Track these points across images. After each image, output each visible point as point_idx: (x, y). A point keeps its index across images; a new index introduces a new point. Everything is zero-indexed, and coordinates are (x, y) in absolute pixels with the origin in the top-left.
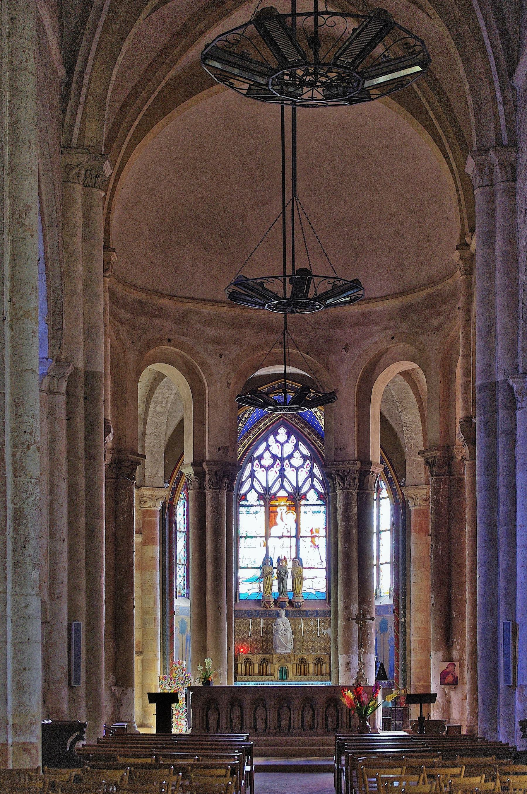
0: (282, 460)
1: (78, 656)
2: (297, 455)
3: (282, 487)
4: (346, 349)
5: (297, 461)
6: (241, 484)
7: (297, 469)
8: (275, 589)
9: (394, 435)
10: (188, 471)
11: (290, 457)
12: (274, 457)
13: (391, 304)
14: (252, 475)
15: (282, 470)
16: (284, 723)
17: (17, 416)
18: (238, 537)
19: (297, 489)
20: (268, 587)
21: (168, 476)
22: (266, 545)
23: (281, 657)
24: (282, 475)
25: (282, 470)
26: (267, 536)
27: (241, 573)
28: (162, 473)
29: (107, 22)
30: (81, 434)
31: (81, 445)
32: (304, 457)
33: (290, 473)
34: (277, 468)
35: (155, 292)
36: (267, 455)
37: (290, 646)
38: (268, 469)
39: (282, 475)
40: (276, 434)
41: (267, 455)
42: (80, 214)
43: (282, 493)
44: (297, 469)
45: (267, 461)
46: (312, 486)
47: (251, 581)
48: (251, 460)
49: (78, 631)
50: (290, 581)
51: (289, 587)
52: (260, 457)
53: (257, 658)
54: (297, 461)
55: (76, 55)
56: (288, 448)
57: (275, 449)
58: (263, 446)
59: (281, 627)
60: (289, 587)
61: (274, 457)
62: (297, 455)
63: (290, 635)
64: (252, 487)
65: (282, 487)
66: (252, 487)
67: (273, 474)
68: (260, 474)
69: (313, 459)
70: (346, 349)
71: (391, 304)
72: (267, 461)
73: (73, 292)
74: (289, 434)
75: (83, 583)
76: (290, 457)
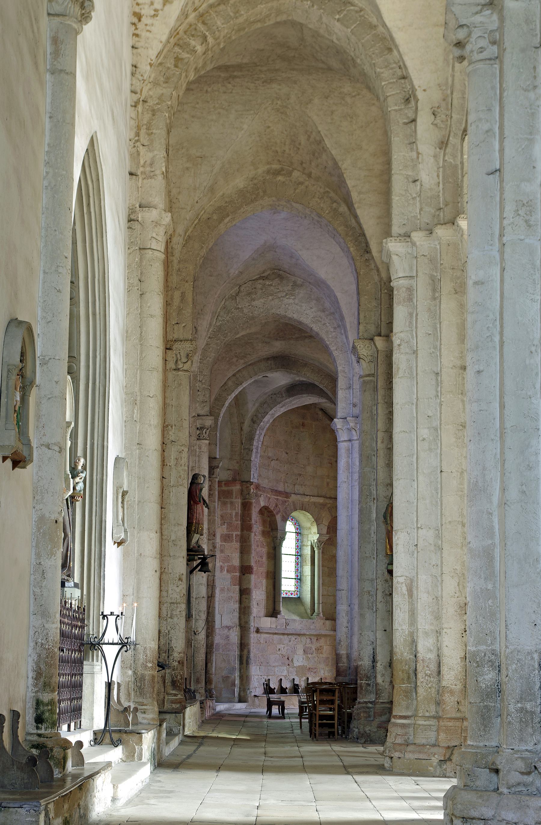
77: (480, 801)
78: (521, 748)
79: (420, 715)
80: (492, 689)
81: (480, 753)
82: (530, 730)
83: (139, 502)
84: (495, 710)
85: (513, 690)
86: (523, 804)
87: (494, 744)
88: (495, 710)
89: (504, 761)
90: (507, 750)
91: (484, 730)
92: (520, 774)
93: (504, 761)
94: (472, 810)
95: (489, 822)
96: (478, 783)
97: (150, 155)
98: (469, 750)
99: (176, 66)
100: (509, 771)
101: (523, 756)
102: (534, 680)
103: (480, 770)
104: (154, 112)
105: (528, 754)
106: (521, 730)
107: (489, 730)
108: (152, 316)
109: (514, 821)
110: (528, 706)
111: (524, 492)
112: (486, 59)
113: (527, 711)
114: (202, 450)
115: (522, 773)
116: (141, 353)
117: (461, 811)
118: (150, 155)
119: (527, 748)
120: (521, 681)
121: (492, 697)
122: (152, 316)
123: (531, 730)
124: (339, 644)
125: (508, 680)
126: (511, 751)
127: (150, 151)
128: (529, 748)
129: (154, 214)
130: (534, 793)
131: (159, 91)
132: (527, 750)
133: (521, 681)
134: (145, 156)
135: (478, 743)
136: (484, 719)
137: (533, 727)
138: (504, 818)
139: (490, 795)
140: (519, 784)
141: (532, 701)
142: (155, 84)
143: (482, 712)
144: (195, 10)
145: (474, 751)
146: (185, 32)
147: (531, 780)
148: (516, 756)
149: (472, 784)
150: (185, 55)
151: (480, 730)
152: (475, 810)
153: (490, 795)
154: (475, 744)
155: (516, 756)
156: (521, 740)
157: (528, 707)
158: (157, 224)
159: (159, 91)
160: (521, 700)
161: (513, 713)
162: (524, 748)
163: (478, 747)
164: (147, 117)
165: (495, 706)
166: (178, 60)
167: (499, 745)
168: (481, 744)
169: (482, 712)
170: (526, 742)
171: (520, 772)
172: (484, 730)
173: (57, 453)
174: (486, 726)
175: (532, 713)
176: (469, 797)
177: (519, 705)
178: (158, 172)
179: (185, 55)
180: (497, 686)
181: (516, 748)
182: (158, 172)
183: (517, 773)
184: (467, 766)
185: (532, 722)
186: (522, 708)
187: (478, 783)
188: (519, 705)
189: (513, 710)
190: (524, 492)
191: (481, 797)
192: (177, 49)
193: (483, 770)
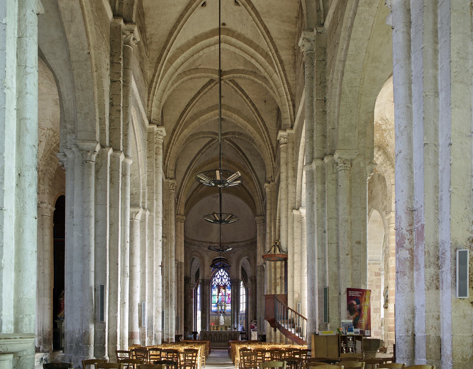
0: (222, 277)
1: (179, 323)
2: (225, 275)
3: (222, 283)
4: (234, 253)
5: (225, 277)
6: (212, 282)
7: (225, 279)
8: (220, 309)
9: (245, 272)
10: (200, 281)
11: (223, 276)
12: (220, 276)
13: (243, 243)
14: (215, 280)
15: (222, 279)
16: (220, 340)
17: (171, 276)
18: (212, 296)
19: (225, 284)
20: (218, 308)
21: (196, 282)
22: (218, 298)
23: (221, 326)
24: (222, 280)
25: (222, 279)
26: (218, 295)
27: (212, 305)
28: (194, 281)
29: (185, 187)
30: (179, 276)
31: (179, 278)
32: (226, 276)
33: (224, 280)
34: (220, 279)
35: (194, 240)
36: (218, 275)
37: (223, 323)
38: (218, 279)
39: (222, 280)
40: (220, 270)
41: (218, 275)
42: (179, 228)
43: (222, 285)
44: (225, 279)
45: (218, 277)
46: (228, 283)
47: (214, 306)
48: (215, 277)
49: (179, 318)
50: (223, 307)
51: (223, 308)
52: (217, 276)
53: (215, 326)
54: (225, 277)
55: (179, 195)
56: (223, 274)
57: (220, 274)
58: (217, 273)
59: (221, 318)
60: (223, 308)
61: (220, 276)
62: (225, 275)
63: (223, 320)
64: (215, 283)
65: (222, 283)
66: (215, 283)
67: (220, 280)
68: (217, 280)
69: (229, 277)
70: (234, 253)
71: (243, 243)
72: (218, 277)
73: (178, 245)
74: (223, 270)
75: (180, 308)
76: (223, 276)
83: (131, 175)
97: (44, 187)
99: (51, 160)
104: (45, 174)
108: (46, 235)
111: (71, 290)
112: (149, 93)
116: (43, 246)
118: (44, 187)
122: (46, 235)
124: (443, 254)
127: (44, 186)
129: (45, 205)
131: (46, 168)
134: (42, 187)
142: (45, 165)
144: (55, 143)
145: (154, 315)
146: (53, 150)
150: (53, 157)
158: (46, 208)
159: (46, 168)
164: (43, 175)
166: (51, 158)
178: (46, 192)
179: (53, 157)
182: (46, 192)
190: (71, 290)
192: (51, 155)
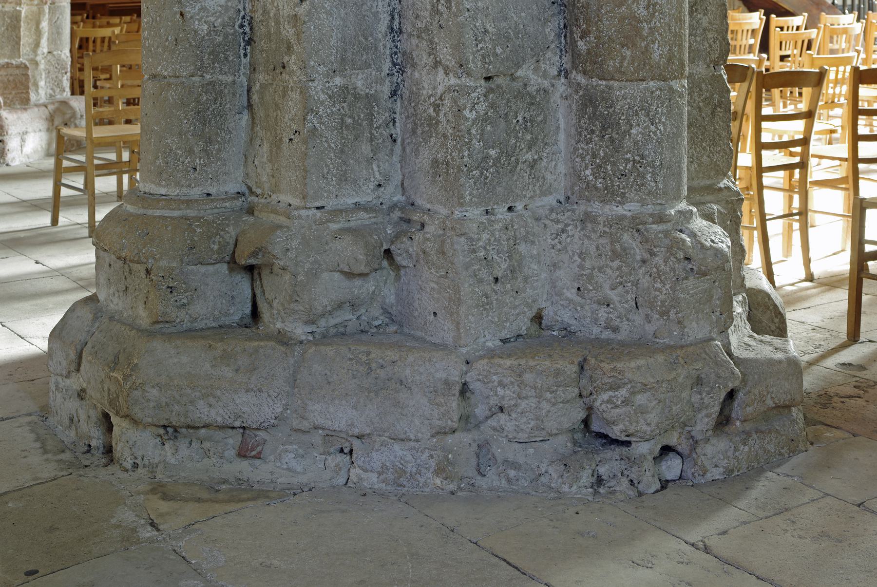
77: (227, 372)
78: (342, 201)
79: (716, 474)
80: (226, 36)
81: (198, 219)
82: (366, 148)
84: (234, 94)
85: (320, 41)
86: (382, 373)
87: (232, 187)
88: (234, 94)
89: (295, 244)
90: (304, 213)
91: (204, 150)
92: (342, 277)
93: (295, 244)
94: (201, 404)
95: (260, 433)
96: (199, 308)
98: (158, 213)
100: (313, 274)
101: (352, 224)
102: (374, 9)
103: (202, 269)
105: (366, 216)
106: (342, 151)
107: (219, 150)
109: (356, 431)
110: (359, 82)
113: (356, 96)
114: (141, 382)
115: (350, 275)
117: (159, 406)
119: (357, 200)
120: (342, 12)
121: (226, 58)
123: (369, 148)
125: (309, 12)
126: (318, 214)
128: (362, 199)
130: (376, 323)
132: (357, 206)
133: (342, 12)
135: (184, 190)
136: (204, 122)
137: (372, 139)
138: (321, 422)
139: (256, 350)
140: (340, 306)
141: (369, 66)
143: (198, 101)
145: (176, 213)
147: (372, 289)
148: (334, 226)
149: (182, 314)
151: (190, 152)
152: (212, 400)
153: (256, 350)
154: (174, 192)
155: (334, 226)
156: (343, 179)
157: (359, 84)
160: (343, 65)
161: (322, 103)
162: (350, 201)
163: (189, 203)
165: (234, 82)
167: (244, 189)
168: (196, 192)
169: (198, 101)
170: (355, 182)
171: (342, 272)
172: (204, 150)
173: (500, 415)
174: (209, 141)
175: (371, 99)
176: (184, 359)
177: (338, 81)
180: (241, 26)
181: (330, 203)
183: (337, 275)
184: (163, 263)
185: (371, 124)
186: (345, 89)
187: (199, 308)
188: (338, 81)
189: (323, 97)
191: (226, 357)
193: (211, 268)
